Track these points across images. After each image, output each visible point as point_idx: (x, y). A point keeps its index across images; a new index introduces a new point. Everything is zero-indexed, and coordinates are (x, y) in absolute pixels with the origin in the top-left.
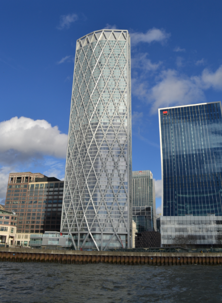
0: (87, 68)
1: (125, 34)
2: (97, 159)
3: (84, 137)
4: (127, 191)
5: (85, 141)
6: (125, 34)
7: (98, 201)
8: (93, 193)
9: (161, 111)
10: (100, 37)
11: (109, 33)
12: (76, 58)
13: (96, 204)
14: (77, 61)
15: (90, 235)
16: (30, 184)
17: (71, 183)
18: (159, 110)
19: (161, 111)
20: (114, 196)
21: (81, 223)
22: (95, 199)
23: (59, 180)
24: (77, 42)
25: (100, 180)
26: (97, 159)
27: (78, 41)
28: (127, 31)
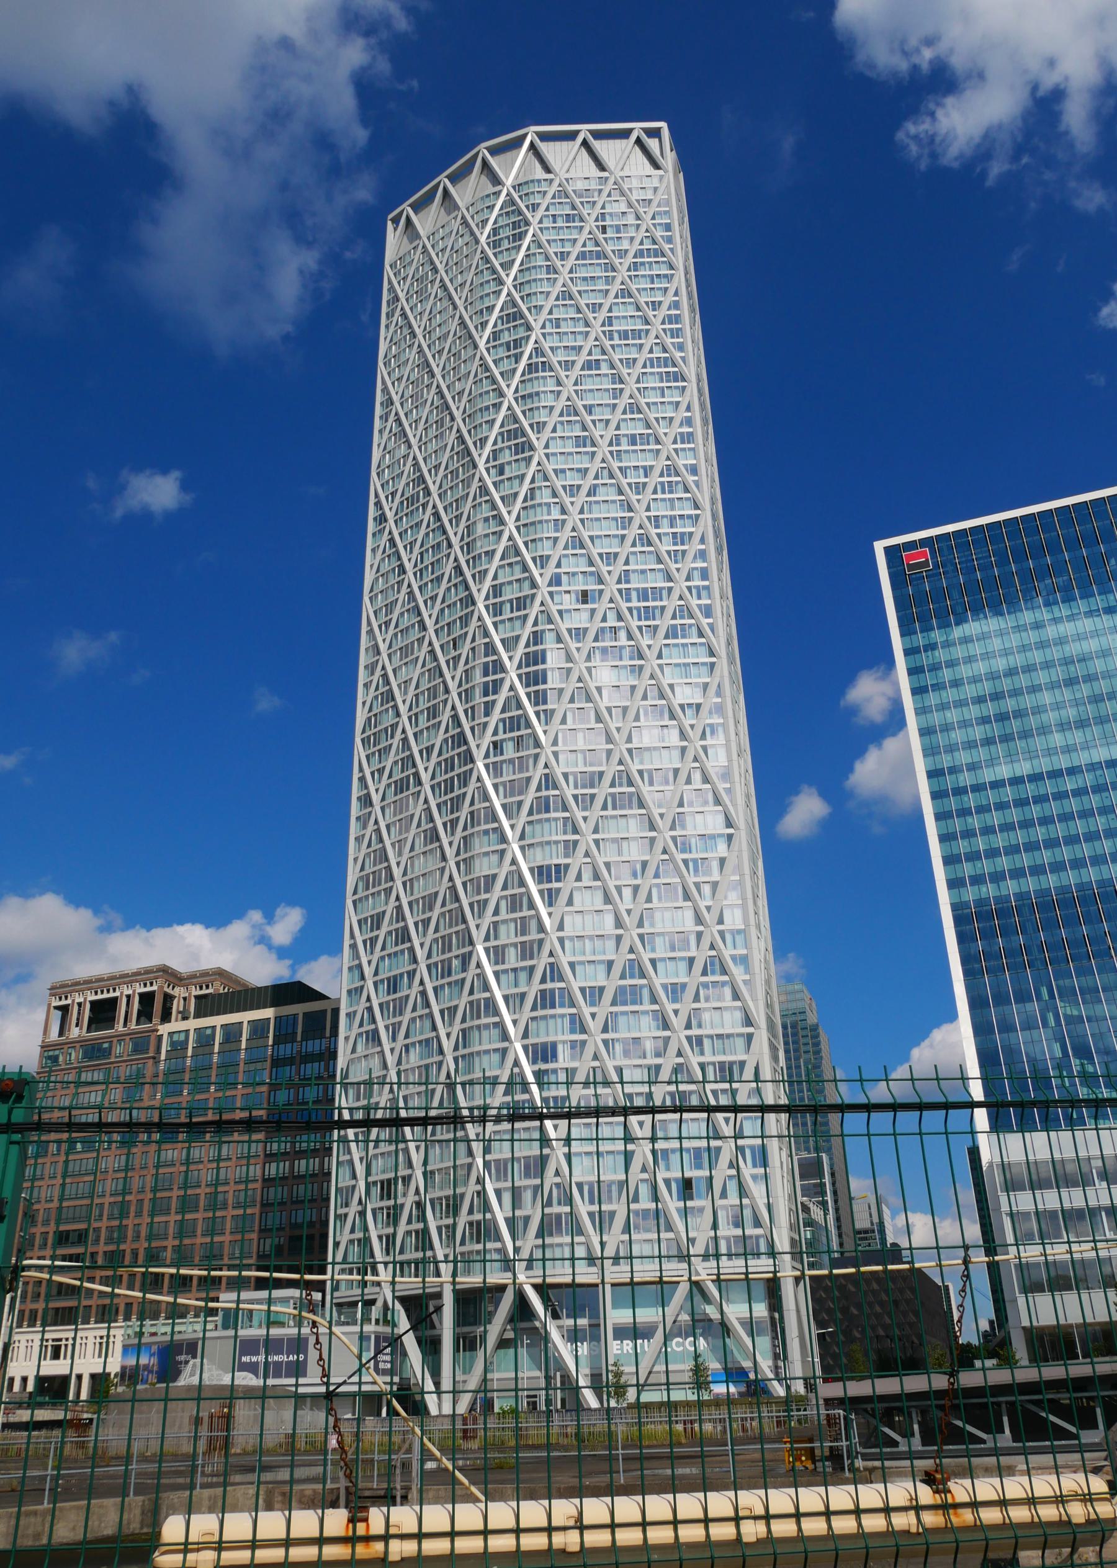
0: (448, 568)
1: (653, 144)
2: (537, 637)
3: (452, 685)
4: (712, 627)
5: (462, 561)
6: (653, 144)
7: (554, 681)
8: (521, 650)
9: (888, 550)
10: (514, 168)
11: (565, 145)
12: (379, 397)
13: (539, 698)
14: (385, 418)
15: (522, 1301)
16: (164, 1029)
17: (391, 798)
18: (879, 546)
19: (888, 550)
20: (652, 827)
21: (463, 1219)
22: (534, 679)
23: (321, 997)
24: (390, 226)
25: (560, 747)
26: (537, 637)
27: (396, 221)
28: (663, 125)
